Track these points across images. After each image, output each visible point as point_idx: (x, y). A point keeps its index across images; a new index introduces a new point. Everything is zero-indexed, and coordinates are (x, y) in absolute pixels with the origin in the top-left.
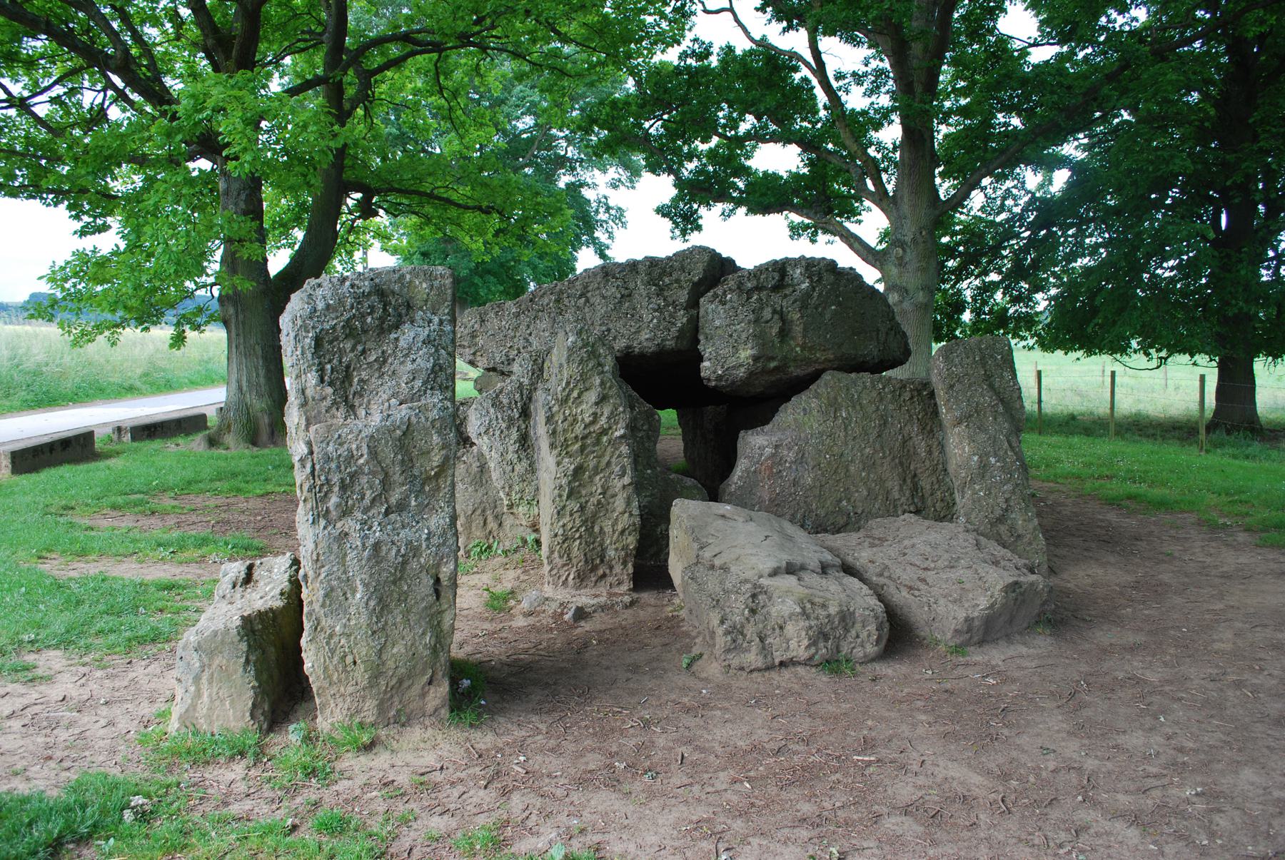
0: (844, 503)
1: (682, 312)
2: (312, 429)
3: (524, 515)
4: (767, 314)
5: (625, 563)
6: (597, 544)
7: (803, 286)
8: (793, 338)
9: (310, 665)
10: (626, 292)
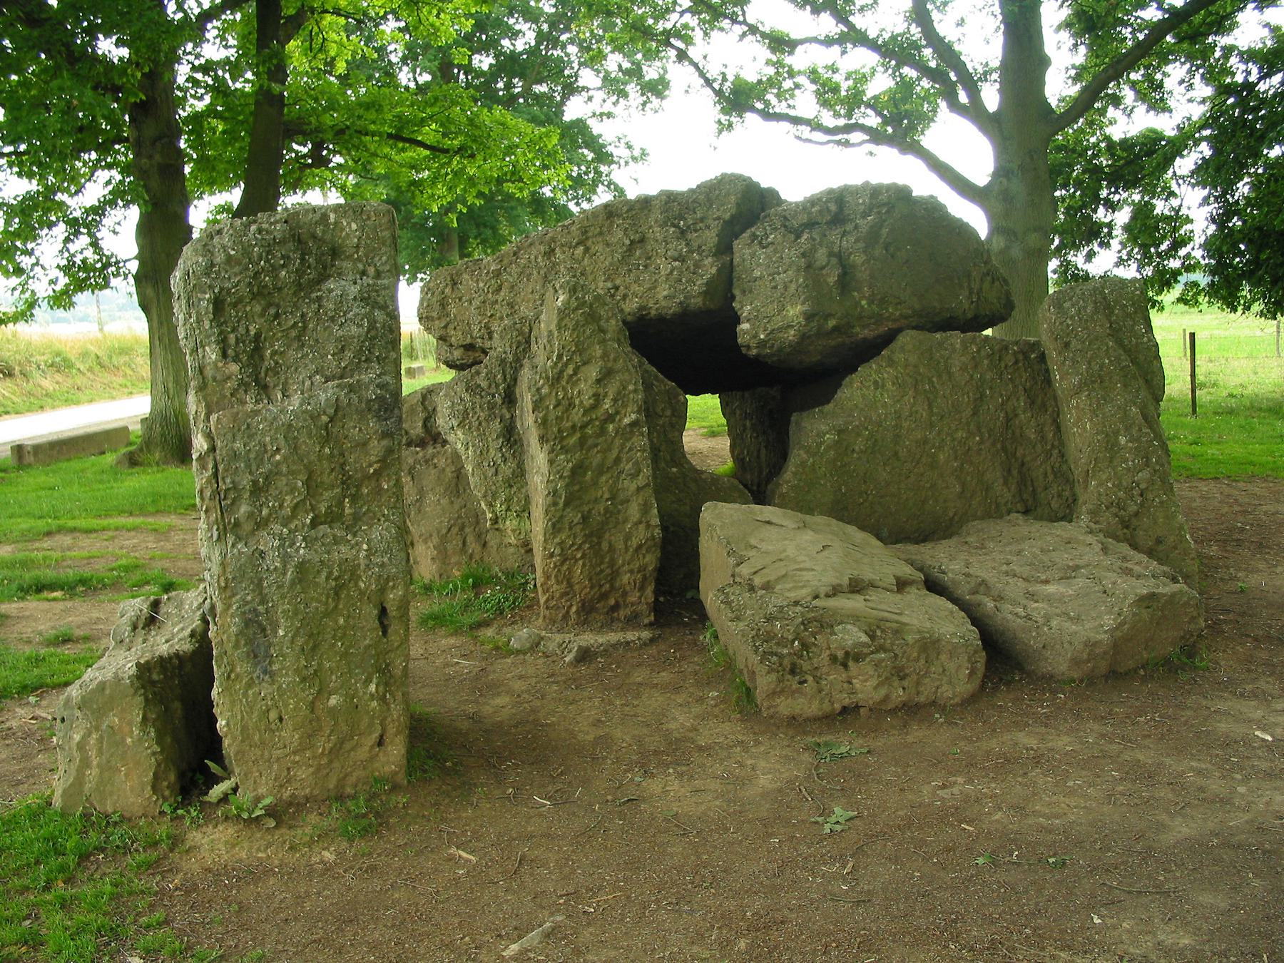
1: (710, 259)
2: (214, 417)
3: (514, 531)
4: (821, 255)
9: (224, 723)
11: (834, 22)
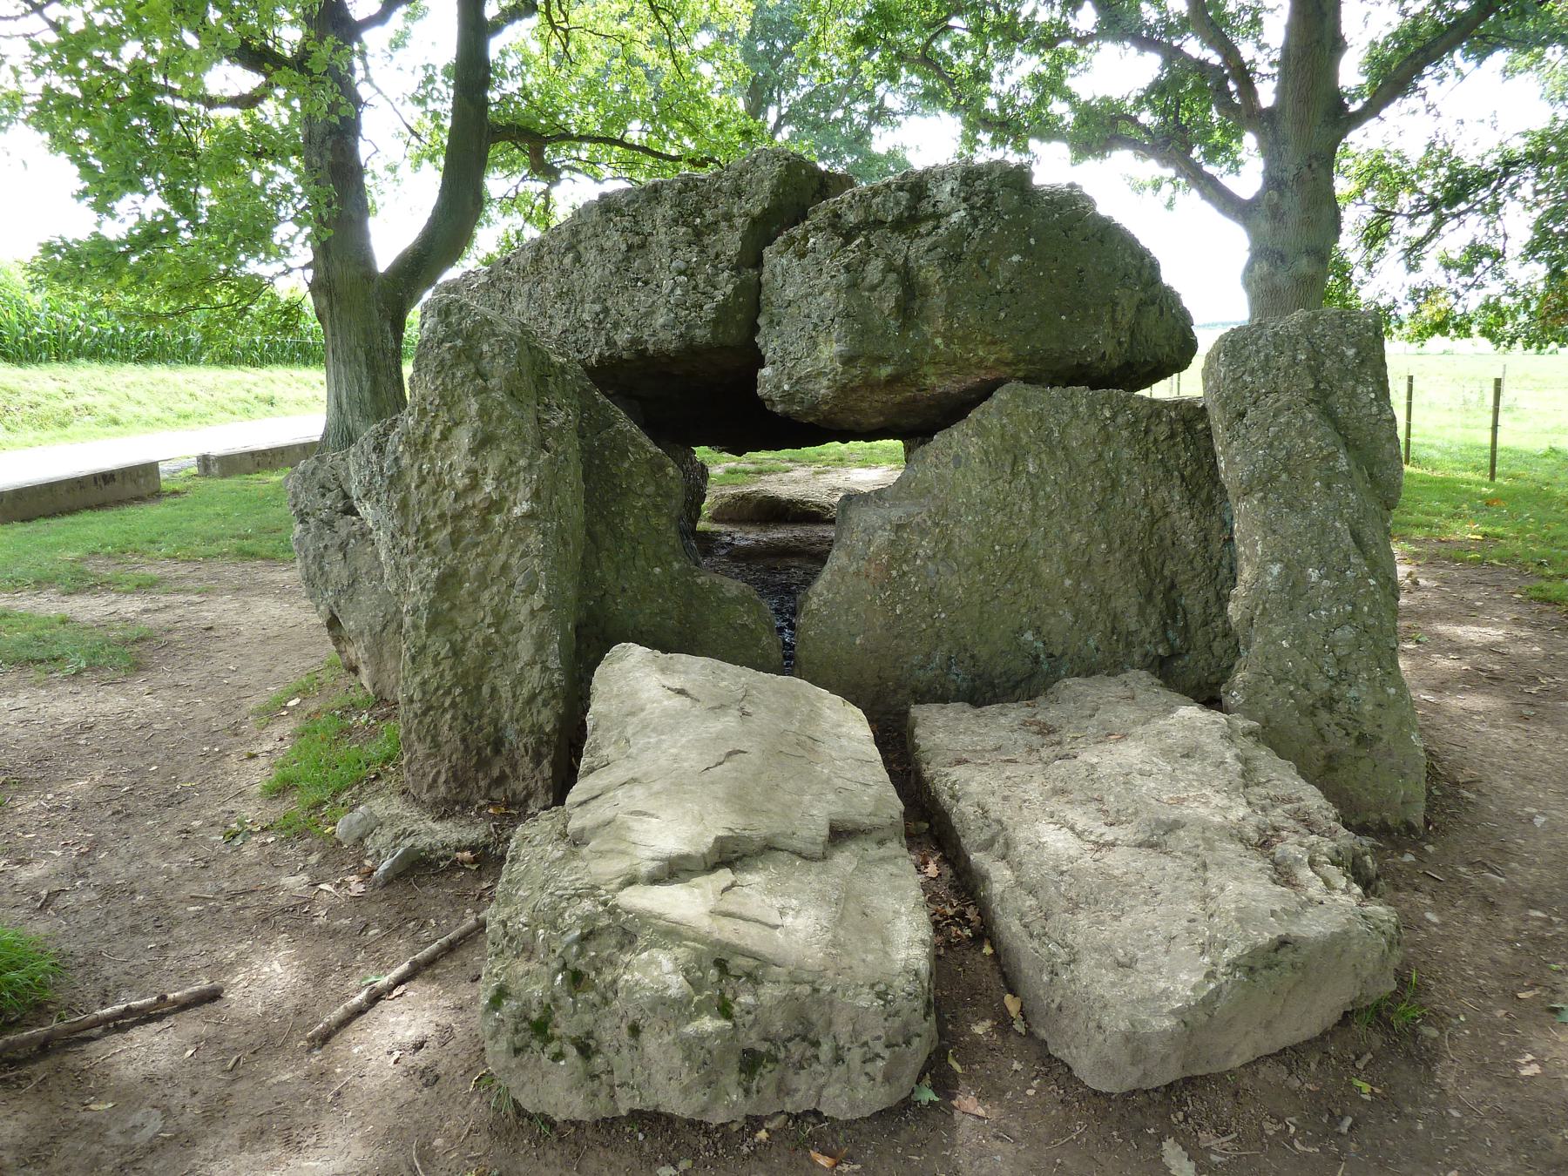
0: (1029, 636)
4: (874, 271)
5: (537, 759)
6: (485, 720)
7: (955, 218)
8: (927, 320)
10: (637, 240)
11: (1375, 120)
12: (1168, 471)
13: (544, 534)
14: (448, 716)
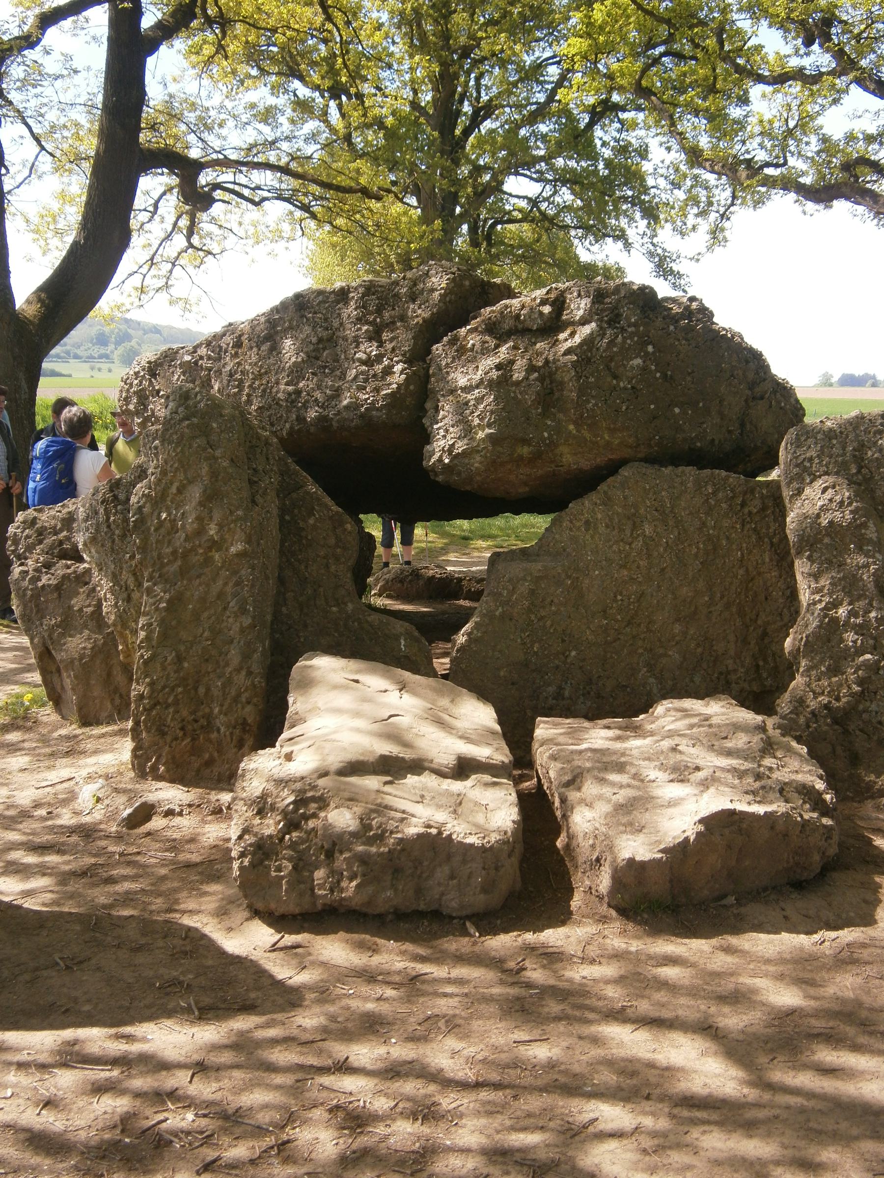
12: (760, 538)
13: (253, 568)
14: (171, 710)
